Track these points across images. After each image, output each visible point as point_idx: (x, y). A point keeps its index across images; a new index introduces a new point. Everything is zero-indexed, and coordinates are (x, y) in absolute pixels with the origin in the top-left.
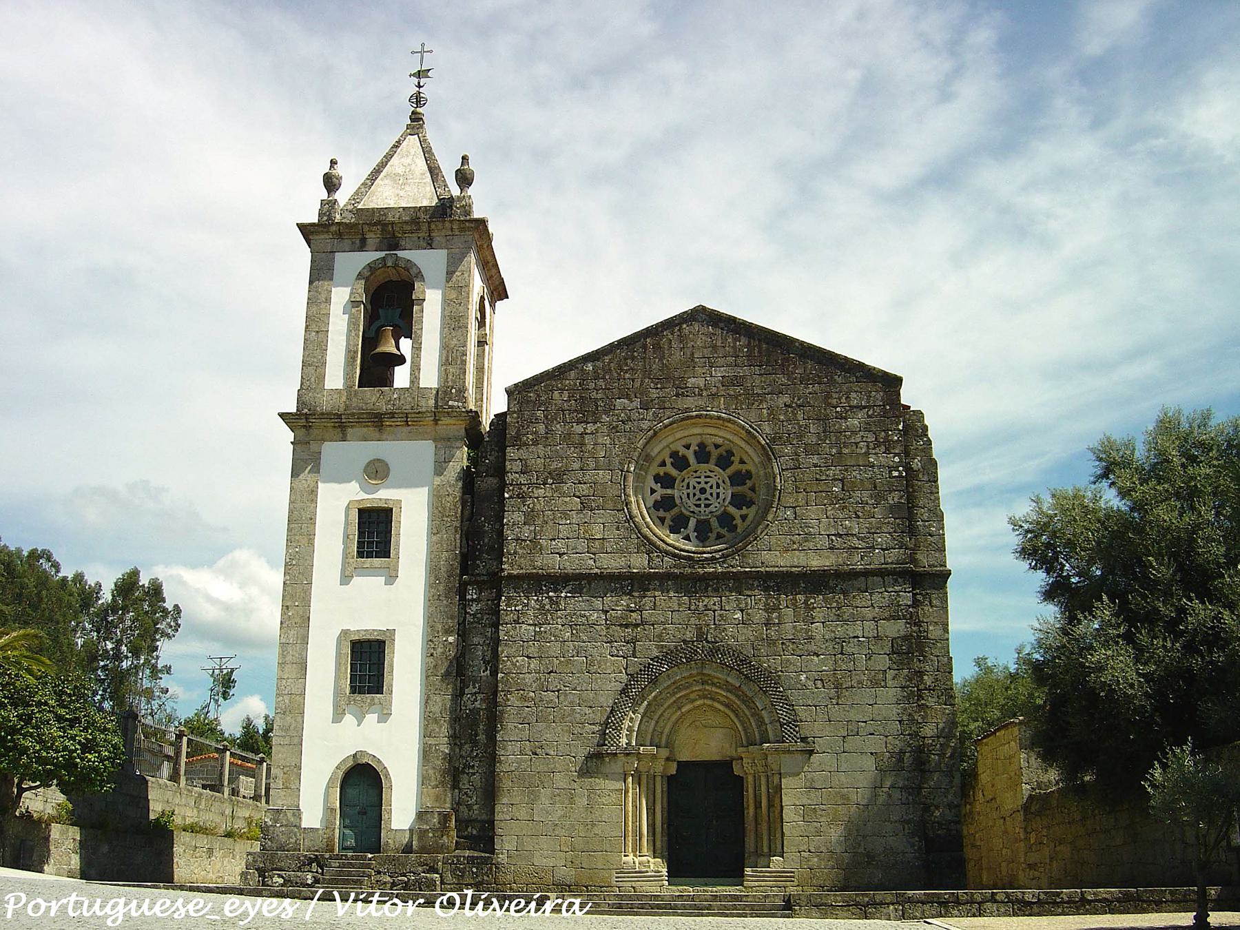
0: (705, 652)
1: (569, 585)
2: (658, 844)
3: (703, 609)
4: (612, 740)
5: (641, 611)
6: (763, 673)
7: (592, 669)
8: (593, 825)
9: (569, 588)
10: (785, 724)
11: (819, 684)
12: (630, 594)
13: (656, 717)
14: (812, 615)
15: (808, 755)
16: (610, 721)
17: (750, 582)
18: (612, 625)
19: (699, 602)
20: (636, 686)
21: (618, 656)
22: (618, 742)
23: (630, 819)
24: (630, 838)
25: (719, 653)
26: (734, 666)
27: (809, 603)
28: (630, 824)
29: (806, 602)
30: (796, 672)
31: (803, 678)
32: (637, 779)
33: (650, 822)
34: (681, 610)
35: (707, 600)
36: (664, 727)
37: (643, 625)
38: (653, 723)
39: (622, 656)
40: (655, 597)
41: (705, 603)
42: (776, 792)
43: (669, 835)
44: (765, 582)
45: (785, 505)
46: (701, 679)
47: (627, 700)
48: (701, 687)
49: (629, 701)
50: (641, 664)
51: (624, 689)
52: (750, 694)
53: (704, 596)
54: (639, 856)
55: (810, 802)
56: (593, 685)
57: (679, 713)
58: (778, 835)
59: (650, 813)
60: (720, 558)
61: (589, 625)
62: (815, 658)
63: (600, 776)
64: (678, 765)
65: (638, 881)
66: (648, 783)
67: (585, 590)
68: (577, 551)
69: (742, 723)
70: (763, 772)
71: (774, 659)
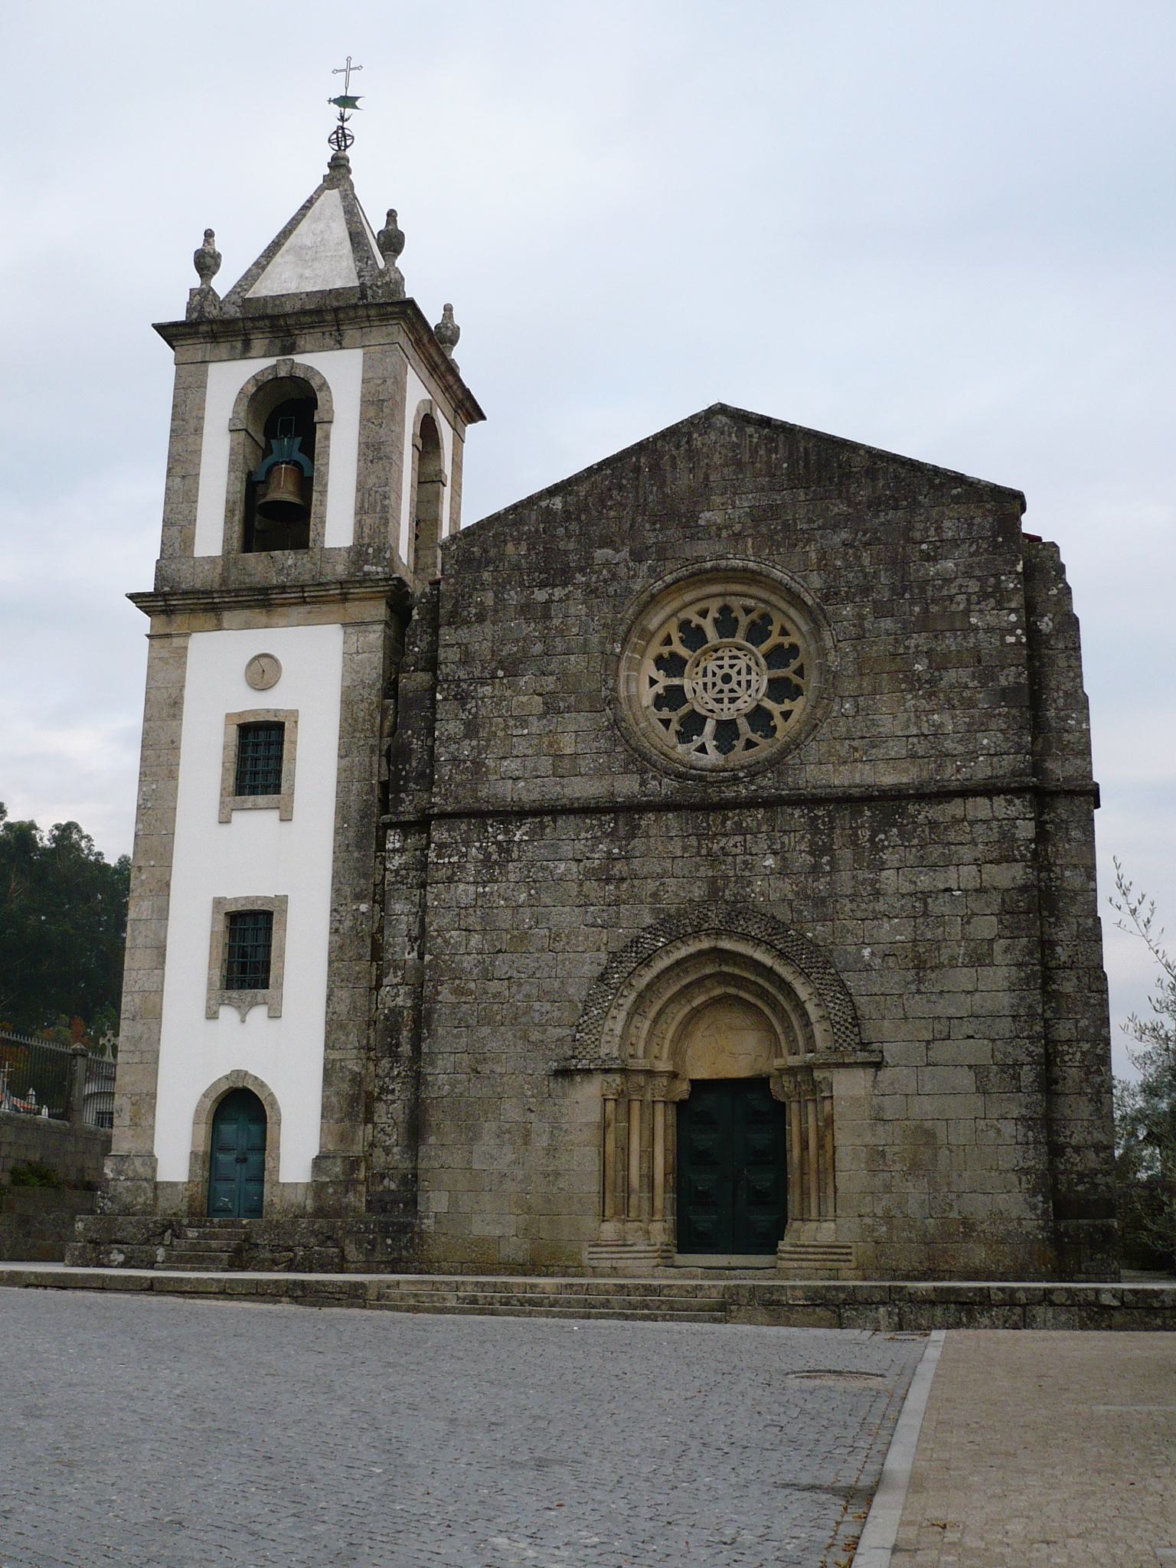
17: (789, 811)
29: (872, 840)
31: (866, 952)
35: (724, 840)
38: (647, 1024)
45: (842, 694)
50: (627, 937)
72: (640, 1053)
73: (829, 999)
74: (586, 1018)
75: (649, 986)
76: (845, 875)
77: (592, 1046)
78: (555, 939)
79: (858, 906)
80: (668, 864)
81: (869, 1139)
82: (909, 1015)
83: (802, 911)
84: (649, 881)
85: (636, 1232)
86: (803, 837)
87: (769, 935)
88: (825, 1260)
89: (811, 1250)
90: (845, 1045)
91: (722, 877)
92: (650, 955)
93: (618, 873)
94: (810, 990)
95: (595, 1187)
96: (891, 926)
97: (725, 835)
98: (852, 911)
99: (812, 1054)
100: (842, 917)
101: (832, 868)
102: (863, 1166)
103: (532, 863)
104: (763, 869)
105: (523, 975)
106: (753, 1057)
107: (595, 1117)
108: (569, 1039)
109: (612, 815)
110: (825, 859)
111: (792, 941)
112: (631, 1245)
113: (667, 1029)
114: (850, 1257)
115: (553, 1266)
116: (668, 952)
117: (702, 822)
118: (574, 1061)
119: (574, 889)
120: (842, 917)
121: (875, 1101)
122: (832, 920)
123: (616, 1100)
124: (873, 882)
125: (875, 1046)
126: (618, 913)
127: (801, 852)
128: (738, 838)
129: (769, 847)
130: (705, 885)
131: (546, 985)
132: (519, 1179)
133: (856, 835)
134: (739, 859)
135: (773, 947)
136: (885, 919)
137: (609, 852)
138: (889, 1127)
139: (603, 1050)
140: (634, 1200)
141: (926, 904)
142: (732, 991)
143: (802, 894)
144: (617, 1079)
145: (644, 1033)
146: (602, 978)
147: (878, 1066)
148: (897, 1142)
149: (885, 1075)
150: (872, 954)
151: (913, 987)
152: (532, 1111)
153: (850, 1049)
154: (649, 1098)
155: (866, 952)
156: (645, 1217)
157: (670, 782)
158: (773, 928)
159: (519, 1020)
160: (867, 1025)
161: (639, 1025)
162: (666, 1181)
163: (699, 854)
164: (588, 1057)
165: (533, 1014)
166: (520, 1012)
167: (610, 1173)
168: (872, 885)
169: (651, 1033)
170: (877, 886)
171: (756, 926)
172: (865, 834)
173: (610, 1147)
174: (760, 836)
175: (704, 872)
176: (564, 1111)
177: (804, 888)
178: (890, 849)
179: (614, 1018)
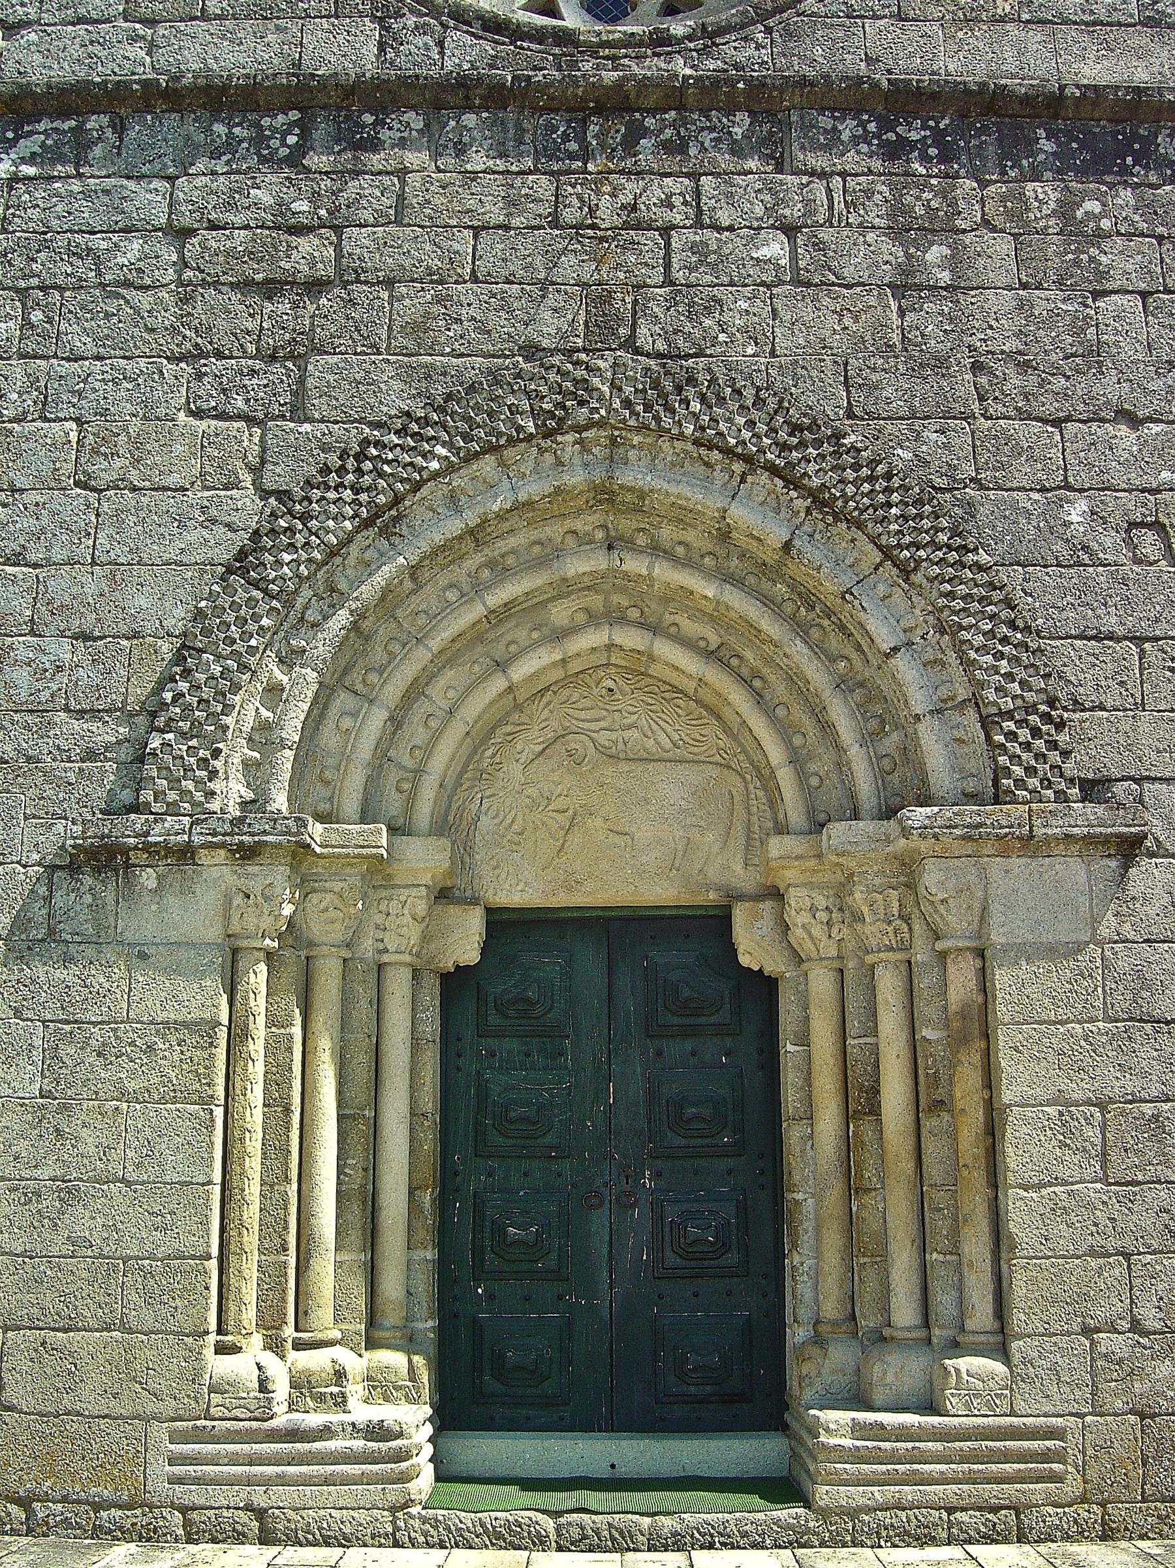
0: (628, 390)
1: (31, 133)
2: (392, 1285)
3: (618, 222)
4: (174, 783)
5: (338, 229)
6: (896, 482)
7: (105, 471)
8: (69, 1194)
9: (27, 146)
10: (1009, 715)
11: (1149, 544)
12: (295, 160)
13: (392, 692)
14: (1092, 259)
15: (1113, 864)
16: (168, 696)
17: (825, 122)
18: (204, 284)
19: (598, 192)
20: (300, 539)
21: (223, 416)
22: (199, 796)
23: (254, 1165)
24: (251, 1269)
25: (690, 392)
26: (762, 451)
27: (1079, 214)
28: (253, 1190)
29: (1065, 210)
30: (1043, 490)
31: (1076, 512)
32: (290, 973)
33: (356, 1178)
34: (516, 222)
35: (632, 187)
36: (429, 748)
37: (345, 284)
38: (377, 719)
39: (239, 417)
40: (402, 173)
41: (625, 198)
42: (958, 1041)
43: (444, 1237)
44: (886, 125)
46: (604, 527)
47: (251, 602)
48: (598, 562)
49: (263, 607)
50: (325, 448)
51: (242, 555)
52: (830, 585)
53: (622, 172)
54: (298, 1346)
55: (1131, 1084)
56: (102, 539)
57: (498, 684)
58: (976, 1245)
59: (354, 1138)
60: (690, 38)
61: (103, 286)
62: (1123, 430)
63: (109, 954)
64: (489, 924)
65: (283, 1480)
66: (346, 999)
67: (97, 151)
68: (82, 11)
69: (784, 731)
70: (890, 949)
71: (941, 432)
73: (979, 640)
90: (1033, 782)
100: (995, 408)
109: (294, 115)
117: (566, 138)
118: (138, 820)
120: (995, 408)
131: (59, 585)
155: (1076, 512)
157: (468, 39)
168: (1078, 328)
175: (570, 268)
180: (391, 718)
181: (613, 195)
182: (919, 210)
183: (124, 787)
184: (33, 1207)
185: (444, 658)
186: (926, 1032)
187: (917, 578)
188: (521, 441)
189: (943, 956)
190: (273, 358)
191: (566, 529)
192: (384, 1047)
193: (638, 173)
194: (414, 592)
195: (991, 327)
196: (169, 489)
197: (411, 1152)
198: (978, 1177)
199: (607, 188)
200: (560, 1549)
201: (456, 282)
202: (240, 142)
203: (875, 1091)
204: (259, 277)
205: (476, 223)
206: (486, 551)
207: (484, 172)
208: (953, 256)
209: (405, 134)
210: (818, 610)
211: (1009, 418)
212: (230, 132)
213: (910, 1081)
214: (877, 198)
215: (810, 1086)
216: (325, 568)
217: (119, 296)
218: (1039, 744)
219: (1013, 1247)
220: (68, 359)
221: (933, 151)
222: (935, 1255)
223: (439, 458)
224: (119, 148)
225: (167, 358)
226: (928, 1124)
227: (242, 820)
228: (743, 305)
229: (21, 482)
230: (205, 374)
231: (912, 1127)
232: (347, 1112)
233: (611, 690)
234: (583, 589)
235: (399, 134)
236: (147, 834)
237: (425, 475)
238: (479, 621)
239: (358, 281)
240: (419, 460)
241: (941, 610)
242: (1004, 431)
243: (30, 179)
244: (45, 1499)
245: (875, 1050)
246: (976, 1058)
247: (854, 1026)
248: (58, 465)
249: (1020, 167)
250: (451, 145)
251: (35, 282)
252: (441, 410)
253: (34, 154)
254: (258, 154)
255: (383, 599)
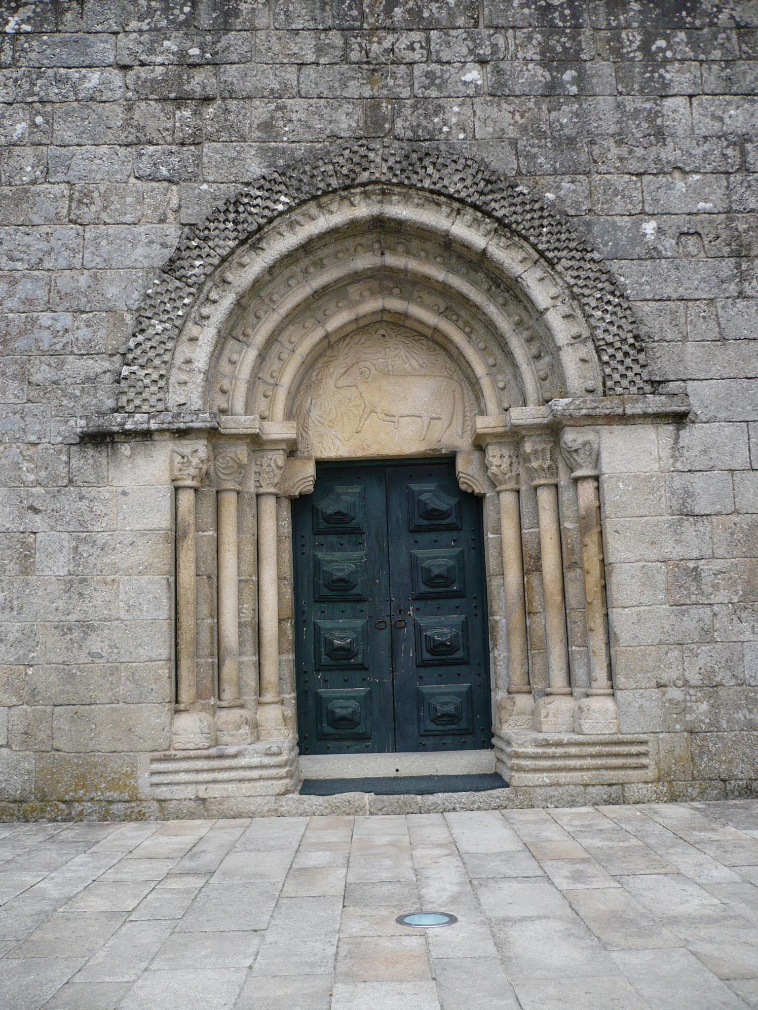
14: (661, 76)
27: (654, 48)
29: (645, 47)
31: (649, 227)
35: (390, 38)
38: (251, 355)
42: (584, 528)
43: (299, 646)
51: (172, 261)
58: (597, 641)
71: (573, 182)
72: (239, 405)
73: (593, 303)
74: (140, 338)
75: (257, 285)
76: (604, 104)
77: (154, 388)
78: (80, 202)
79: (631, 152)
80: (290, 75)
81: (671, 549)
82: (731, 333)
83: (535, 156)
84: (257, 102)
85: (239, 728)
86: (529, 38)
87: (482, 193)
88: (597, 768)
89: (573, 750)
90: (625, 383)
91: (388, 99)
92: (260, 228)
93: (198, 89)
94: (553, 291)
95: (164, 651)
96: (688, 187)
97: (393, 30)
98: (621, 159)
99: (566, 400)
100: (602, 168)
101: (581, 89)
102: (661, 596)
103: (39, 69)
104: (461, 88)
105: (18, 265)
106: (426, 420)
107: (163, 520)
108: (108, 378)
110: (568, 75)
111: (523, 203)
112: (235, 756)
113: (282, 370)
114: (644, 761)
115: (80, 801)
116: (292, 225)
117: (350, 8)
118: (119, 417)
119: (116, 115)
120: (602, 168)
121: (678, 483)
122: (587, 173)
123: (196, 490)
124: (652, 116)
125: (672, 387)
126: (199, 157)
127: (526, 61)
128: (417, 36)
129: (471, 51)
130: (360, 112)
131: (64, 281)
132: (11, 637)
133: (619, 39)
134: (418, 70)
135: (488, 214)
136: (677, 174)
137: (182, 54)
138: (704, 526)
139: (175, 397)
140: (229, 669)
141: (744, 153)
142: (395, 304)
143: (533, 129)
144: (200, 448)
145: (245, 370)
146: (171, 267)
147: (680, 419)
148: (720, 552)
149: (691, 435)
150: (660, 230)
151: (733, 288)
152: (36, 511)
153: (634, 389)
154: (251, 487)
155: (649, 227)
156: (250, 697)
158: (488, 182)
159: (11, 346)
160: (658, 350)
161: (235, 357)
162: (281, 632)
163: (345, 59)
164: (145, 408)
165: (37, 333)
166: (14, 331)
167: (187, 621)
169: (255, 378)
170: (659, 121)
171: (456, 178)
172: (633, 39)
173: (187, 575)
174: (454, 33)
175: (354, 89)
176: (98, 508)
177: (536, 120)
178: (677, 65)
179: (193, 340)
180: (259, 355)
181: (379, 43)
182: (559, 49)
183: (109, 398)
184: (69, 637)
185: (288, 319)
186: (567, 525)
187: (559, 268)
188: (330, 192)
189: (576, 480)
190: (183, 144)
191: (356, 243)
192: (262, 541)
193: (394, 29)
194: (270, 281)
195: (601, 119)
196: (126, 224)
197: (279, 599)
198: (597, 604)
199: (375, 39)
200: (371, 814)
201: (289, 98)
202: (155, 11)
203: (538, 558)
204: (172, 95)
205: (298, 61)
206: (311, 257)
207: (303, 29)
208: (579, 76)
209: (255, 6)
210: (502, 287)
211: (610, 173)
212: (149, 5)
213: (557, 551)
214: (534, 42)
215: (502, 556)
216: (219, 269)
217: (88, 107)
218: (628, 361)
219: (617, 640)
220: (60, 146)
221: (567, 12)
222: (574, 648)
223: (284, 203)
224: (82, 14)
225: (120, 145)
226: (570, 575)
227: (179, 414)
228: (456, 109)
229: (36, 220)
230: (143, 154)
231: (560, 577)
232: (242, 578)
233: (383, 336)
234: (367, 278)
235: (251, 6)
236: (124, 424)
237: (275, 213)
238: (308, 298)
239: (231, 97)
240: (269, 203)
241: (573, 286)
242: (608, 181)
243: (28, 33)
244: (80, 801)
245: (538, 536)
246: (595, 537)
247: (526, 522)
248: (58, 210)
249: (619, 20)
250: (282, 13)
251: (36, 98)
252: (283, 174)
253: (29, 18)
254: (167, 18)
255: (253, 286)
